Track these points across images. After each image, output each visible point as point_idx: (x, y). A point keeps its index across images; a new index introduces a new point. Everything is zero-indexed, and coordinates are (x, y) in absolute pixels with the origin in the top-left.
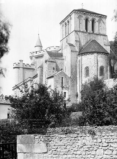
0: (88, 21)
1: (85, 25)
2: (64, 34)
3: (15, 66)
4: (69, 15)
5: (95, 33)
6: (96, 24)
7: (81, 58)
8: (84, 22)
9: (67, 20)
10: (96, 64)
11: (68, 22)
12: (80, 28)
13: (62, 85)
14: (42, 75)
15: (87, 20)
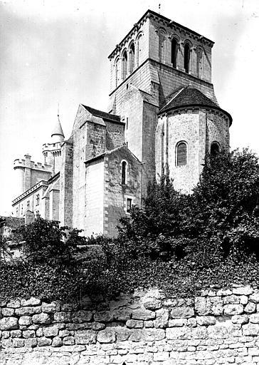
0: (177, 47)
1: (170, 51)
2: (120, 76)
3: (17, 164)
4: (136, 27)
5: (190, 73)
6: (193, 55)
7: (167, 121)
8: (168, 45)
9: (130, 40)
10: (205, 136)
11: (132, 47)
12: (160, 55)
13: (123, 182)
14: (72, 163)
15: (174, 43)
